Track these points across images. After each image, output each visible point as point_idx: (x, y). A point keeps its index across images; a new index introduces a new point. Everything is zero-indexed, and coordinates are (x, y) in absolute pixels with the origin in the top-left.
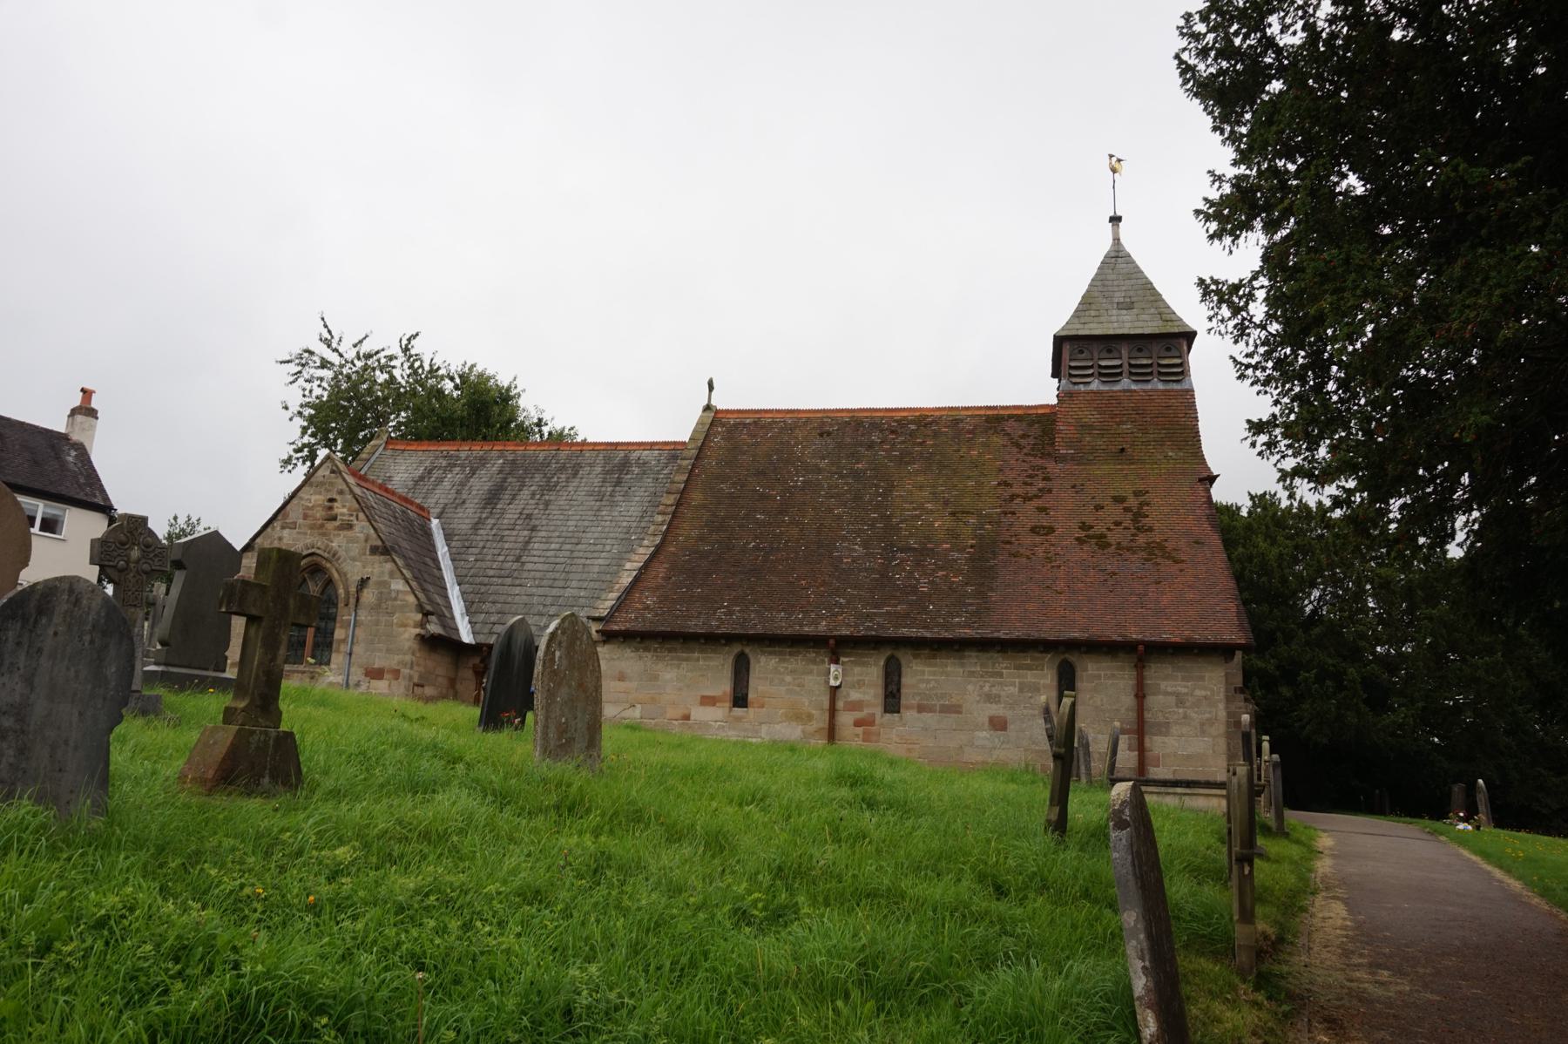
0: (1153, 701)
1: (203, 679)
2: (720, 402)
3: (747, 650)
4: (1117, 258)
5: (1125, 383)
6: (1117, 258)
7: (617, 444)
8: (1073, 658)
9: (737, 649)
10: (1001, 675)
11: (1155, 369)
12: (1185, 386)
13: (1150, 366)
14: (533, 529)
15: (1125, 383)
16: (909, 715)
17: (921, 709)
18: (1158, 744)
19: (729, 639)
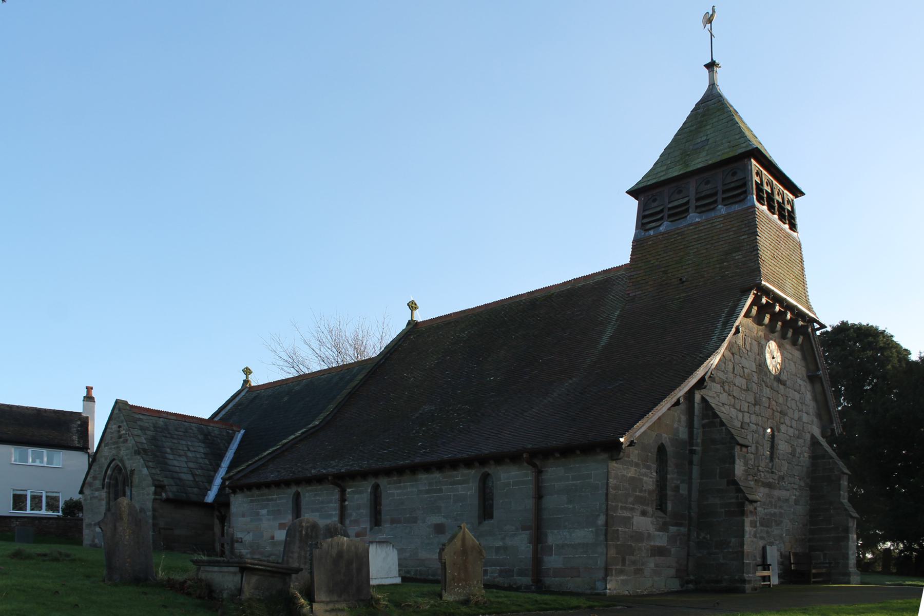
0: (551, 502)
1: (218, 562)
2: (420, 317)
3: (299, 490)
4: (712, 111)
5: (694, 217)
6: (712, 111)
7: (804, 283)
8: (491, 469)
9: (294, 489)
10: (441, 490)
11: (666, 213)
12: (750, 204)
13: (662, 211)
14: (120, 437)
15: (694, 217)
16: (386, 526)
17: (393, 521)
18: (553, 538)
19: (287, 483)
